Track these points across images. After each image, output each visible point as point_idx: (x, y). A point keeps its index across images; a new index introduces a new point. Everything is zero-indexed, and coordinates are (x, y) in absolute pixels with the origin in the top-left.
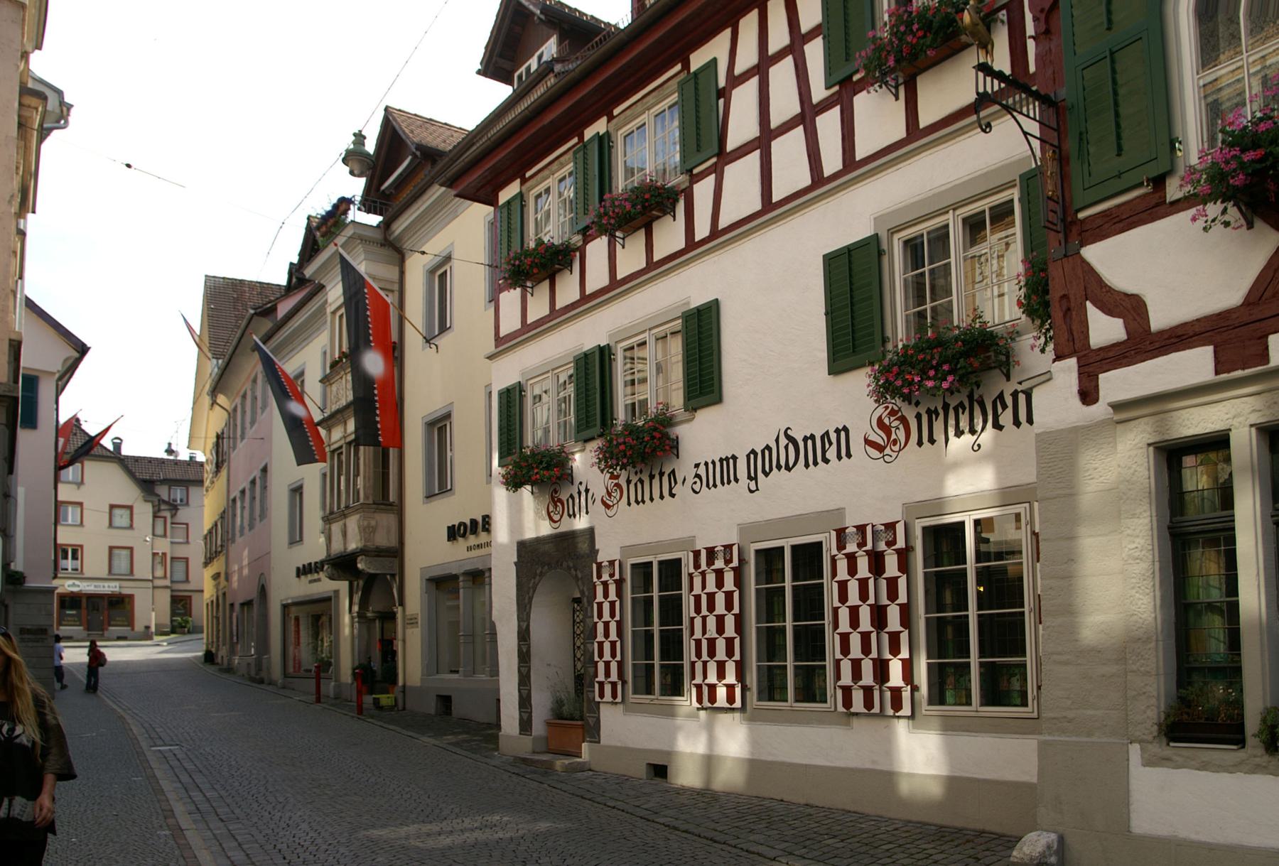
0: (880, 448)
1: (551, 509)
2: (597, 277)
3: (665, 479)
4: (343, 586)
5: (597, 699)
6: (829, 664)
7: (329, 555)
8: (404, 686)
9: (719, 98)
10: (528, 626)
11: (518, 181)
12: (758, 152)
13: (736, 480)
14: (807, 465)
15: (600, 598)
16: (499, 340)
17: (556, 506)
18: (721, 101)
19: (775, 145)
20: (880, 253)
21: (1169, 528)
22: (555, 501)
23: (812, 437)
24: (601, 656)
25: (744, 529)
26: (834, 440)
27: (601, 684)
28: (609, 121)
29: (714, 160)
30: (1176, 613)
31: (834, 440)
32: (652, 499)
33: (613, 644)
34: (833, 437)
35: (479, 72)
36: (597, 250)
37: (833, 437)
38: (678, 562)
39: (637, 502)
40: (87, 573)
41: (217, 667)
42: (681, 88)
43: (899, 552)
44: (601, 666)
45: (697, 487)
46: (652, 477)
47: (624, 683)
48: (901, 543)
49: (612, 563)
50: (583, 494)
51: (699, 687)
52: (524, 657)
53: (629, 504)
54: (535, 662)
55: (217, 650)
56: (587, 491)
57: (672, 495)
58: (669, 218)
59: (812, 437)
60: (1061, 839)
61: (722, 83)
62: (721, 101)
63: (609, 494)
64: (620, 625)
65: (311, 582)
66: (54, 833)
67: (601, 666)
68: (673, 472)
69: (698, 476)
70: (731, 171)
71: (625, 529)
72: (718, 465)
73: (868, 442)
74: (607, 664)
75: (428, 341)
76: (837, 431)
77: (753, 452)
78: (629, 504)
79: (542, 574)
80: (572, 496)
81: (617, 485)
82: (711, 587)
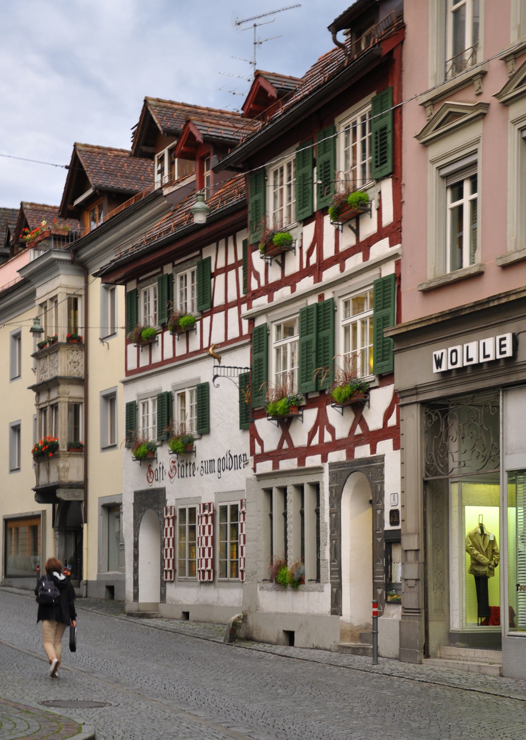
1: (149, 475)
4: (48, 508)
7: (38, 485)
9: (211, 278)
14: (235, 469)
15: (166, 526)
22: (150, 471)
24: (166, 557)
27: (166, 571)
29: (209, 309)
32: (187, 476)
34: (242, 456)
37: (242, 456)
38: (195, 508)
42: (199, 265)
44: (166, 562)
45: (202, 472)
46: (187, 465)
49: (171, 507)
50: (161, 469)
51: (199, 571)
56: (163, 468)
57: (194, 475)
58: (194, 333)
61: (213, 270)
62: (213, 280)
63: (172, 471)
64: (213, 538)
67: (166, 562)
68: (194, 464)
69: (202, 467)
71: (179, 491)
72: (185, 475)
74: (169, 560)
76: (244, 455)
77: (219, 459)
79: (144, 511)
80: (157, 469)
81: (174, 466)
82: (204, 523)
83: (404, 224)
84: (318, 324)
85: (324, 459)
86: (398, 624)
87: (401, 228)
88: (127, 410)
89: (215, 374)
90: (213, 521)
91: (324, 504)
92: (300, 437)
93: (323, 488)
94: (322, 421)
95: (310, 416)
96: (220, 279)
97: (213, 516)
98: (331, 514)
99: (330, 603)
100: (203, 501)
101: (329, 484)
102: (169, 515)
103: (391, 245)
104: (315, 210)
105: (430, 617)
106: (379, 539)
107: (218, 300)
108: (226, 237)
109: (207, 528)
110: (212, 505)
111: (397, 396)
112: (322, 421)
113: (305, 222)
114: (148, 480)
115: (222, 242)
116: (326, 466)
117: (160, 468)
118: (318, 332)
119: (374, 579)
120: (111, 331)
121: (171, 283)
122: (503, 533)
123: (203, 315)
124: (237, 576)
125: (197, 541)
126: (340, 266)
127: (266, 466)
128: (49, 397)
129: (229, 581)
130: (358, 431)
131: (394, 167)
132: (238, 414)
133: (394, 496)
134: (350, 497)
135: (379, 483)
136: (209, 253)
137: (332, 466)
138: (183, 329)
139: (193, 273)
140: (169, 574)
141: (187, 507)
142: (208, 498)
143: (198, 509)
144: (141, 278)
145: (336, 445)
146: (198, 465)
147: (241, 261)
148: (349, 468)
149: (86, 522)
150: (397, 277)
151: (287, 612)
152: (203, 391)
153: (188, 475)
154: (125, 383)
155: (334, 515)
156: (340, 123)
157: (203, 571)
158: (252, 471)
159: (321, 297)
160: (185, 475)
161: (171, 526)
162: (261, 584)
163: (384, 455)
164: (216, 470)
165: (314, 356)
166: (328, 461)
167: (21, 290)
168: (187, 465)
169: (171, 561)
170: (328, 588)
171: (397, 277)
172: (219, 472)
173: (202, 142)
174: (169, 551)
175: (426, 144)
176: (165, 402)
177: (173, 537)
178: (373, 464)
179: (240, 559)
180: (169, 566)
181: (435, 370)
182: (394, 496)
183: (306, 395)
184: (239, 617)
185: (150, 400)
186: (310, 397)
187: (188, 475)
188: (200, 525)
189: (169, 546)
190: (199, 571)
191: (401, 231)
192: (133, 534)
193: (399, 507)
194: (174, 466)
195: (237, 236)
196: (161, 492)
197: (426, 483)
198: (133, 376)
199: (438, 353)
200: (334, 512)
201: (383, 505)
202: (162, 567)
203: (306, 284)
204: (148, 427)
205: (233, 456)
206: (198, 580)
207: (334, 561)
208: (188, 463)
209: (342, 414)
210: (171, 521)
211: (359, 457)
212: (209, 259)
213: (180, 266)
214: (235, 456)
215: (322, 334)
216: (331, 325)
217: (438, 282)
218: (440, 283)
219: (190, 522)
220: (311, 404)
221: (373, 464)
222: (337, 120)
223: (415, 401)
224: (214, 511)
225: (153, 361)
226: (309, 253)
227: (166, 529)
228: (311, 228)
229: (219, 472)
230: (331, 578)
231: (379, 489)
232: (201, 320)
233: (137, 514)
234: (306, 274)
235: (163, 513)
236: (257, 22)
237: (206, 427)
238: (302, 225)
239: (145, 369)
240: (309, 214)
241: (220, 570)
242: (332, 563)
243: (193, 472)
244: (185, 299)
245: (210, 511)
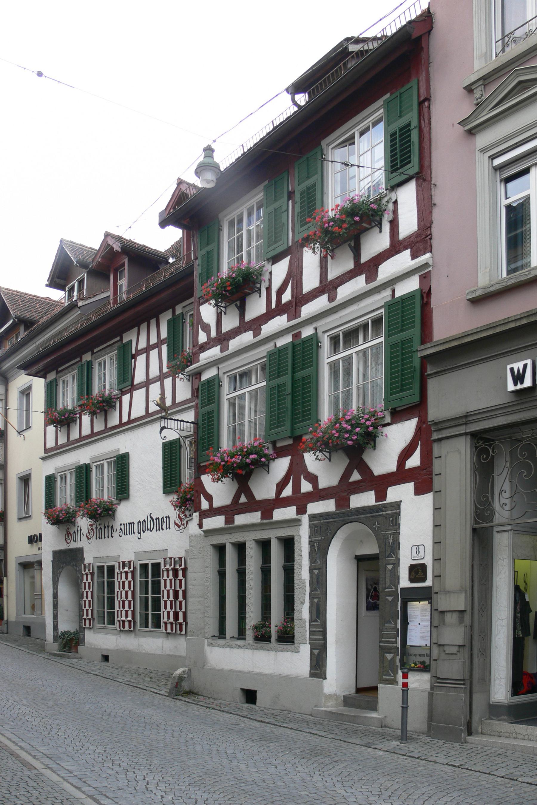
0: (179, 527)
2: (86, 431)
3: (110, 528)
5: (84, 626)
6: (161, 613)
8: (7, 620)
10: (57, 592)
11: (55, 371)
12: (151, 344)
13: (134, 533)
14: (157, 530)
15: (85, 580)
16: (46, 450)
17: (68, 536)
19: (151, 386)
20: (180, 447)
21: (237, 570)
22: (68, 533)
23: (158, 518)
24: (85, 607)
25: (137, 554)
26: (165, 521)
27: (85, 619)
28: (92, 355)
29: (130, 387)
30: (220, 599)
31: (165, 521)
33: (130, 602)
34: (165, 519)
35: (47, 285)
36: (86, 419)
37: (165, 519)
38: (113, 566)
39: (100, 538)
42: (119, 349)
43: (183, 569)
44: (85, 611)
45: (121, 534)
47: (94, 619)
48: (183, 566)
49: (89, 564)
51: (119, 621)
52: (55, 606)
54: (60, 610)
56: (81, 530)
57: (112, 537)
59: (158, 518)
60: (190, 670)
61: (134, 352)
62: (133, 360)
63: (89, 533)
66: (47, 523)
67: (85, 611)
68: (112, 526)
69: (121, 529)
70: (136, 393)
71: (94, 552)
72: (103, 537)
73: (176, 524)
74: (87, 610)
75: (19, 433)
76: (166, 517)
77: (140, 522)
78: (96, 538)
79: (63, 568)
80: (75, 532)
81: (92, 529)
82: (124, 579)
83: (435, 230)
84: (293, 364)
85: (302, 510)
87: (431, 234)
88: (46, 481)
89: (162, 426)
90: (133, 577)
91: (301, 560)
92: (264, 488)
93: (300, 543)
94: (297, 470)
95: (281, 466)
96: (141, 360)
97: (133, 573)
98: (311, 570)
99: (309, 665)
100: (122, 559)
101: (310, 537)
102: (87, 571)
103: (414, 256)
104: (290, 244)
105: (474, 691)
107: (139, 377)
110: (132, 562)
112: (297, 470)
115: (144, 326)
116: (305, 519)
117: (78, 531)
118: (293, 372)
120: (26, 426)
121: (90, 368)
122: (472, 595)
123: (123, 393)
124: (159, 627)
125: (161, 596)
126: (329, 296)
129: (150, 631)
130: (356, 476)
131: (421, 166)
132: (161, 480)
134: (338, 552)
135: (391, 534)
136: (130, 336)
137: (312, 517)
138: (104, 406)
140: (87, 622)
141: (106, 565)
142: (126, 557)
143: (117, 566)
144: (59, 369)
145: (319, 495)
146: (117, 527)
147: (165, 339)
148: (342, 519)
149: (6, 576)
150: (425, 295)
151: (246, 670)
152: (122, 463)
153: (106, 536)
154: (43, 459)
155: (316, 572)
156: (328, 145)
157: (124, 622)
158: (197, 527)
159: (297, 336)
160: (103, 537)
161: (89, 580)
162: (209, 641)
163: (401, 501)
164: (136, 531)
165: (289, 399)
166: (308, 513)
168: (105, 527)
169: (90, 611)
170: (305, 650)
171: (425, 295)
172: (139, 533)
173: (120, 250)
174: (87, 602)
175: (471, 133)
176: (83, 473)
177: (91, 590)
178: (380, 513)
179: (164, 612)
180: (87, 615)
181: (511, 387)
183: (274, 443)
184: (184, 672)
185: (67, 472)
186: (279, 445)
187: (106, 536)
189: (87, 598)
190: (119, 621)
191: (431, 239)
192: (52, 587)
193: (428, 561)
194: (92, 529)
195: (160, 321)
196: (80, 551)
197: (474, 530)
198: (50, 453)
199: (518, 366)
200: (317, 567)
202: (81, 615)
203: (280, 322)
204: (66, 496)
206: (118, 629)
208: (106, 525)
209: (330, 460)
210: (89, 576)
211: (358, 505)
213: (99, 353)
215: (299, 375)
216: (314, 364)
217: (504, 284)
218: (509, 284)
219: (108, 578)
220: (280, 453)
221: (380, 513)
222: (324, 143)
223: (464, 432)
224: (134, 568)
225: (71, 439)
227: (85, 583)
229: (139, 533)
230: (310, 638)
231: (391, 541)
233: (55, 570)
234: (275, 314)
237: (126, 493)
238: (271, 263)
239: (62, 446)
240: (285, 247)
241: (140, 621)
243: (112, 534)
244: (105, 379)
245: (130, 568)
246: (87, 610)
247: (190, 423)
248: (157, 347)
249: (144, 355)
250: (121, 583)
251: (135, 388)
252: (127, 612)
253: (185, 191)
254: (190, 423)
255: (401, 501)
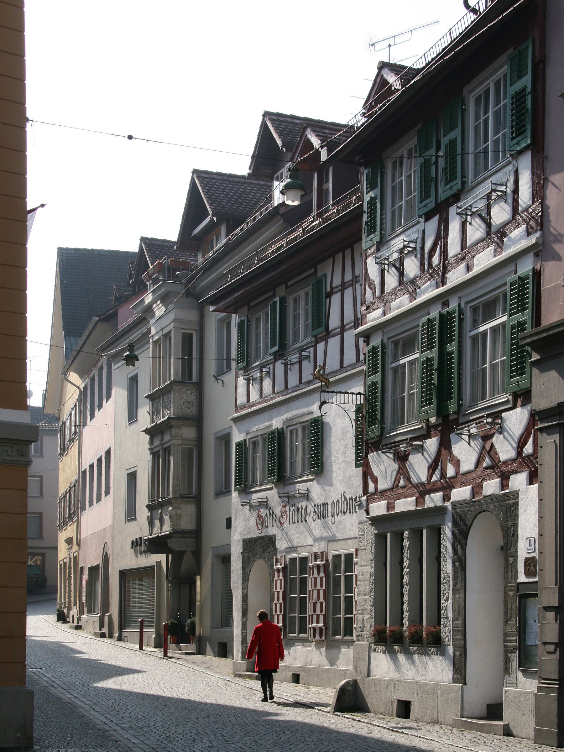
9: (326, 298)
15: (276, 578)
18: (328, 300)
24: (276, 612)
32: (298, 522)
40: (373, 654)
41: (68, 625)
44: (276, 617)
45: (314, 518)
53: (290, 523)
55: (69, 610)
65: (132, 477)
67: (276, 617)
69: (315, 511)
74: (278, 616)
77: (333, 502)
78: (290, 523)
81: (285, 511)
82: (316, 575)
86: (532, 698)
96: (336, 299)
106: (511, 593)
107: (334, 322)
108: (342, 250)
109: (319, 580)
110: (324, 554)
111: (534, 417)
113: (428, 217)
114: (258, 528)
115: (339, 256)
119: (505, 641)
127: (379, 508)
128: (162, 440)
133: (530, 540)
136: (325, 269)
139: (307, 295)
156: (470, 92)
158: (365, 514)
164: (330, 514)
167: (138, 328)
172: (333, 516)
174: (278, 606)
182: (530, 540)
188: (311, 577)
193: (536, 555)
201: (517, 551)
205: (348, 498)
207: (457, 620)
212: (325, 275)
214: (351, 499)
222: (466, 89)
226: (431, 253)
227: (276, 581)
228: (434, 223)
229: (333, 516)
232: (315, 347)
235: (273, 563)
236: (391, 42)
242: (455, 622)
246: (278, 616)
247: (356, 394)
248: (352, 285)
249: (339, 294)
250: (313, 579)
251: (330, 335)
252: (318, 616)
253: (412, 67)
254: (356, 394)
255: (519, 491)
